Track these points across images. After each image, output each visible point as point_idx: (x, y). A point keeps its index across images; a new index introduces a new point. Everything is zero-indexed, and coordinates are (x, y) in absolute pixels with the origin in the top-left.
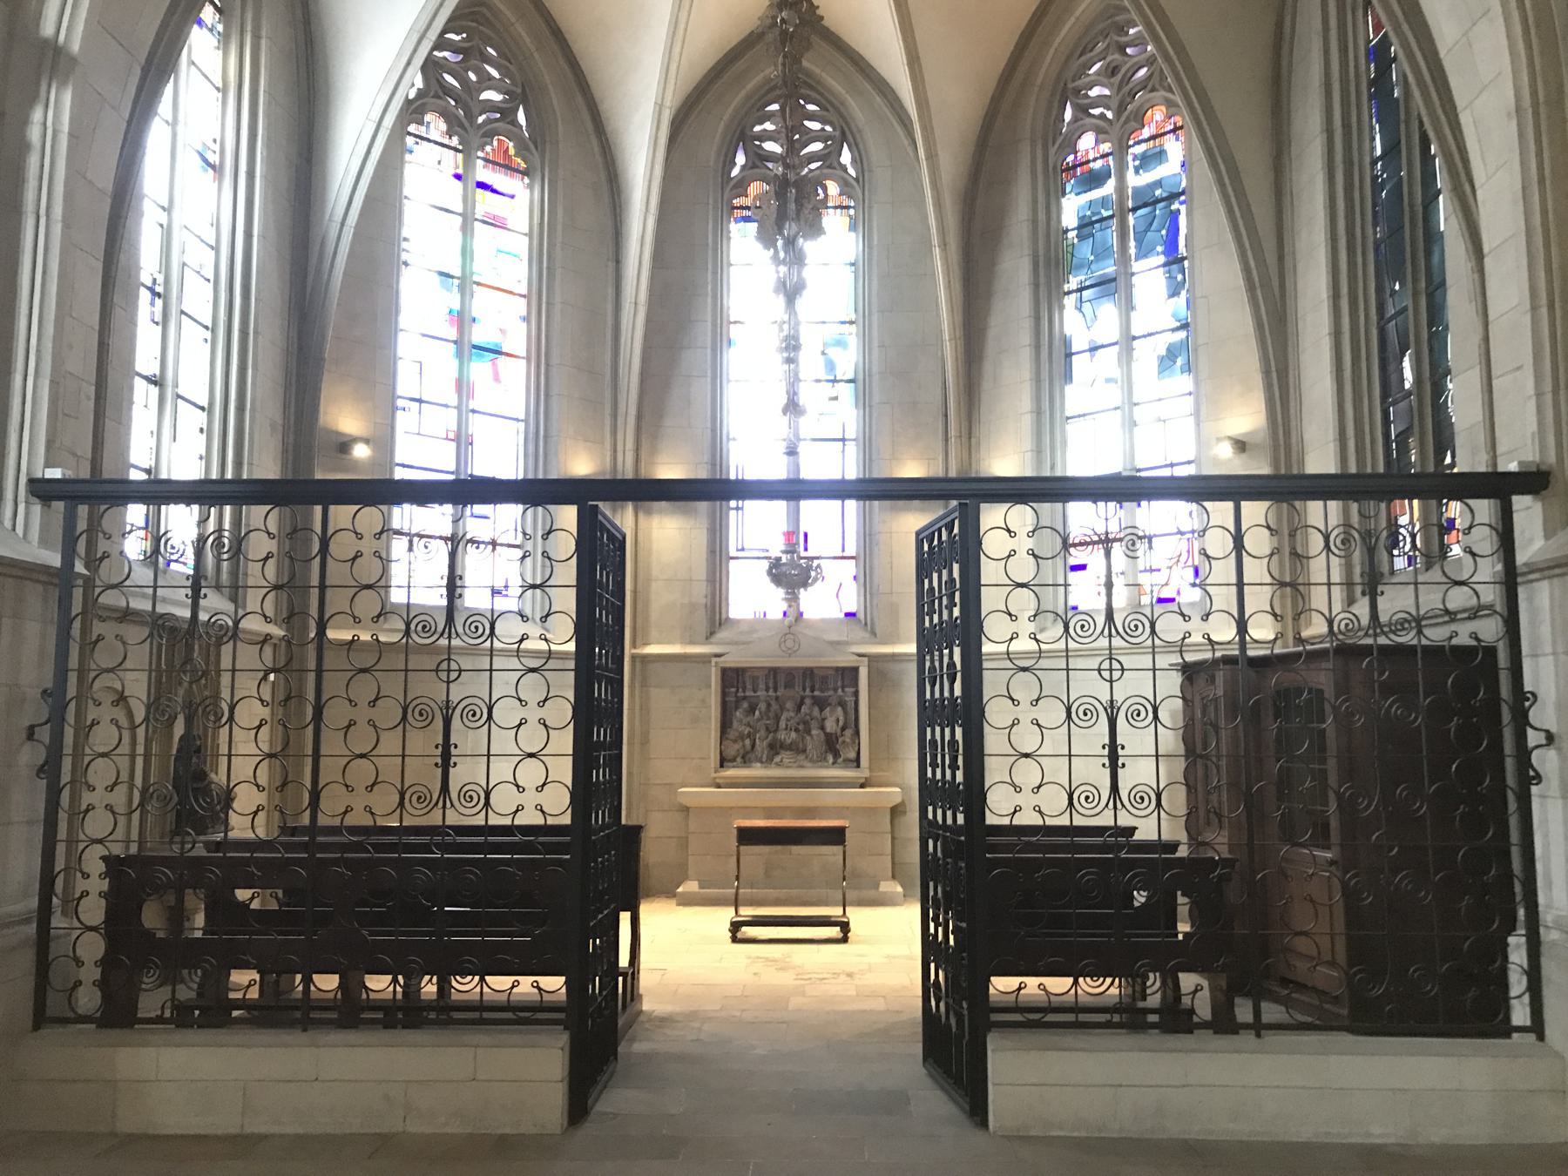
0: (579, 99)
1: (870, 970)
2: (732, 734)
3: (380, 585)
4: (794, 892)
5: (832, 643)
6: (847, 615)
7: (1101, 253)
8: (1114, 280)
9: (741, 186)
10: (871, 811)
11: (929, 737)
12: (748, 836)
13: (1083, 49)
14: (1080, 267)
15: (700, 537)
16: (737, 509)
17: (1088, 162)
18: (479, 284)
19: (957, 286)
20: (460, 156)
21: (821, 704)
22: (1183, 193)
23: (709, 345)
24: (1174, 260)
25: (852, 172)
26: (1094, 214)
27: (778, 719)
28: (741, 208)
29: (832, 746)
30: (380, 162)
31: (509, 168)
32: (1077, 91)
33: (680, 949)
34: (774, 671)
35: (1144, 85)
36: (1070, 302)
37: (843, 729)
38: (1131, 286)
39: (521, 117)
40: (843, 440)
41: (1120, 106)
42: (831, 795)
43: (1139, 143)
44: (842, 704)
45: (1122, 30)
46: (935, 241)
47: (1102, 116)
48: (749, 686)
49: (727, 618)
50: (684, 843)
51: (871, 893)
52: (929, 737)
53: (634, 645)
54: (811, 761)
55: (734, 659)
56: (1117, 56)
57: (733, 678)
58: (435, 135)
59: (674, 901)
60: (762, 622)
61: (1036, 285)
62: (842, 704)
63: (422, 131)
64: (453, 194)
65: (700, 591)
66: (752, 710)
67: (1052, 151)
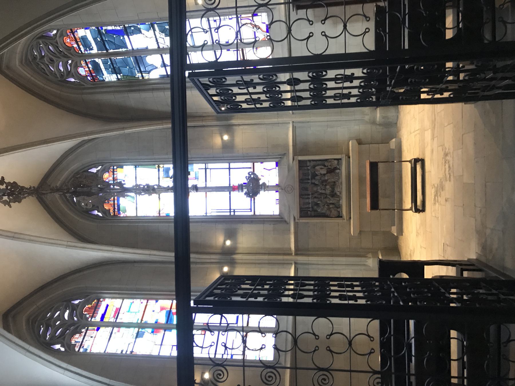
0: (69, 278)
1: (443, 145)
2: (328, 213)
3: (264, 365)
4: (396, 185)
5: (289, 170)
6: (277, 166)
7: (125, 63)
8: (136, 57)
9: (106, 212)
10: (360, 153)
11: (355, 283)
12: (375, 206)
13: (44, 74)
14: (132, 72)
15: (246, 227)
16: (234, 212)
17: (90, 70)
18: (142, 320)
19: (142, 123)
20: (90, 328)
21: (314, 176)
22: (98, 28)
23: (167, 224)
24: (126, 32)
25: (100, 167)
26: (110, 67)
27: (321, 194)
28: (114, 212)
29: (333, 170)
30: (79, 367)
31: (96, 308)
32: (62, 76)
33: (430, 238)
34: (301, 196)
35: (56, 47)
36: (146, 76)
37: (325, 166)
38: (138, 49)
39: (77, 302)
40: (206, 169)
41: (65, 57)
42: (354, 170)
43: (80, 49)
44: (314, 167)
45: (35, 58)
46: (122, 132)
47: (70, 65)
48: (307, 206)
49: (279, 215)
50: (375, 233)
51: (396, 154)
52: (355, 283)
53: (291, 254)
54: (339, 179)
55: (296, 212)
56: (45, 59)
57: (304, 213)
58: (80, 340)
59: (400, 237)
60: (280, 201)
61: (139, 90)
62: (314, 167)
63: (78, 345)
64: (105, 331)
65: (269, 227)
66: (317, 204)
67: (86, 86)
